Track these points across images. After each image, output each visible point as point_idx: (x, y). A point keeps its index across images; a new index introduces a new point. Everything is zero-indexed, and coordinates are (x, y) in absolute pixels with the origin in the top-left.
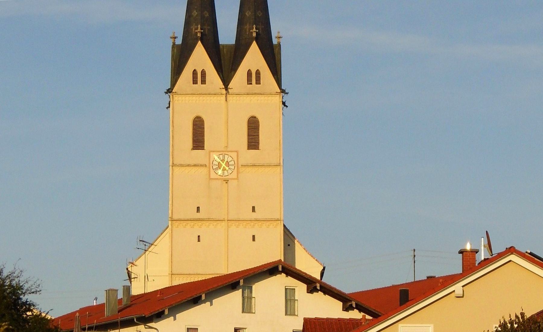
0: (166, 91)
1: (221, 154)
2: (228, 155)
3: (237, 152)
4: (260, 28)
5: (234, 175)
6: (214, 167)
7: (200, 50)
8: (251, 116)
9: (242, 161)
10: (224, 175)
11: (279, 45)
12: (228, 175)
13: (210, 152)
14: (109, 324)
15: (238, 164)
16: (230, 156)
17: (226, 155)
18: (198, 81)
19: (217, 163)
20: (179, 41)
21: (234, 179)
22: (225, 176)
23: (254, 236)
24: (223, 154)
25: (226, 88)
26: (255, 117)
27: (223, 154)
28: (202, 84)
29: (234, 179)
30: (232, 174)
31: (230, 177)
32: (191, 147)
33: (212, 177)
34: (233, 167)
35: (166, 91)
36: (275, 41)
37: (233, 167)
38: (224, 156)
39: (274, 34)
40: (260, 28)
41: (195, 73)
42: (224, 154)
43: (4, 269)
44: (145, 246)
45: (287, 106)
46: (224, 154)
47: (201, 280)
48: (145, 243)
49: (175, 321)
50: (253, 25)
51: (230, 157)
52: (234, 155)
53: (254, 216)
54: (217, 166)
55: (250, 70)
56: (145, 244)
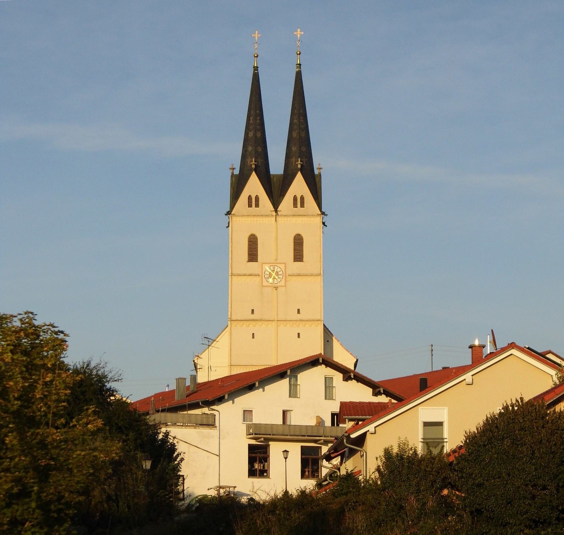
0: (226, 213)
3: (285, 263)
5: (282, 283)
9: (289, 272)
11: (320, 175)
13: (263, 264)
15: (285, 274)
17: (276, 266)
19: (269, 273)
20: (237, 172)
23: (299, 334)
26: (300, 235)
34: (281, 277)
35: (226, 213)
36: (316, 172)
37: (281, 277)
38: (274, 267)
39: (316, 166)
41: (250, 198)
45: (326, 226)
52: (282, 266)
53: (299, 317)
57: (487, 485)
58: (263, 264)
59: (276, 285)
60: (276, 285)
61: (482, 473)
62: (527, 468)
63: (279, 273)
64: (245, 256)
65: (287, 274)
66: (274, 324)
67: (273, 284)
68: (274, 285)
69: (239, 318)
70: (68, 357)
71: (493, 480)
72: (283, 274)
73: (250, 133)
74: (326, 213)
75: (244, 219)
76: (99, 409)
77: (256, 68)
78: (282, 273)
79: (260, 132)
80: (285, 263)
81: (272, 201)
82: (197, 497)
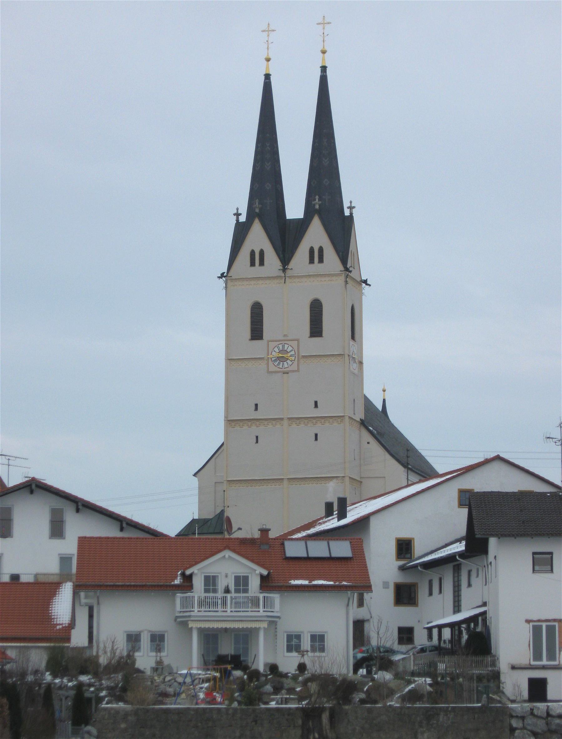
0: (220, 276)
1: (281, 344)
2: (288, 345)
3: (298, 340)
4: (327, 199)
5: (295, 367)
7: (257, 229)
8: (312, 300)
11: (351, 216)
14: (513, 536)
15: (298, 355)
17: (285, 345)
19: (288, 350)
20: (243, 219)
21: (293, 371)
22: (284, 368)
23: (316, 435)
24: (282, 344)
25: (284, 270)
29: (293, 371)
30: (292, 366)
31: (290, 369)
35: (220, 276)
36: (347, 213)
38: (284, 345)
39: (346, 204)
40: (327, 199)
44: (8, 460)
45: (370, 285)
48: (7, 458)
49: (268, 527)
50: (316, 196)
51: (274, 349)
56: (8, 458)
58: (268, 341)
59: (285, 370)
60: (285, 370)
64: (247, 333)
65: (300, 356)
69: (10, 469)
70: (386, 388)
72: (295, 354)
73: (266, 163)
77: (324, 69)
78: (294, 354)
79: (270, 163)
81: (282, 256)
82: (443, 579)
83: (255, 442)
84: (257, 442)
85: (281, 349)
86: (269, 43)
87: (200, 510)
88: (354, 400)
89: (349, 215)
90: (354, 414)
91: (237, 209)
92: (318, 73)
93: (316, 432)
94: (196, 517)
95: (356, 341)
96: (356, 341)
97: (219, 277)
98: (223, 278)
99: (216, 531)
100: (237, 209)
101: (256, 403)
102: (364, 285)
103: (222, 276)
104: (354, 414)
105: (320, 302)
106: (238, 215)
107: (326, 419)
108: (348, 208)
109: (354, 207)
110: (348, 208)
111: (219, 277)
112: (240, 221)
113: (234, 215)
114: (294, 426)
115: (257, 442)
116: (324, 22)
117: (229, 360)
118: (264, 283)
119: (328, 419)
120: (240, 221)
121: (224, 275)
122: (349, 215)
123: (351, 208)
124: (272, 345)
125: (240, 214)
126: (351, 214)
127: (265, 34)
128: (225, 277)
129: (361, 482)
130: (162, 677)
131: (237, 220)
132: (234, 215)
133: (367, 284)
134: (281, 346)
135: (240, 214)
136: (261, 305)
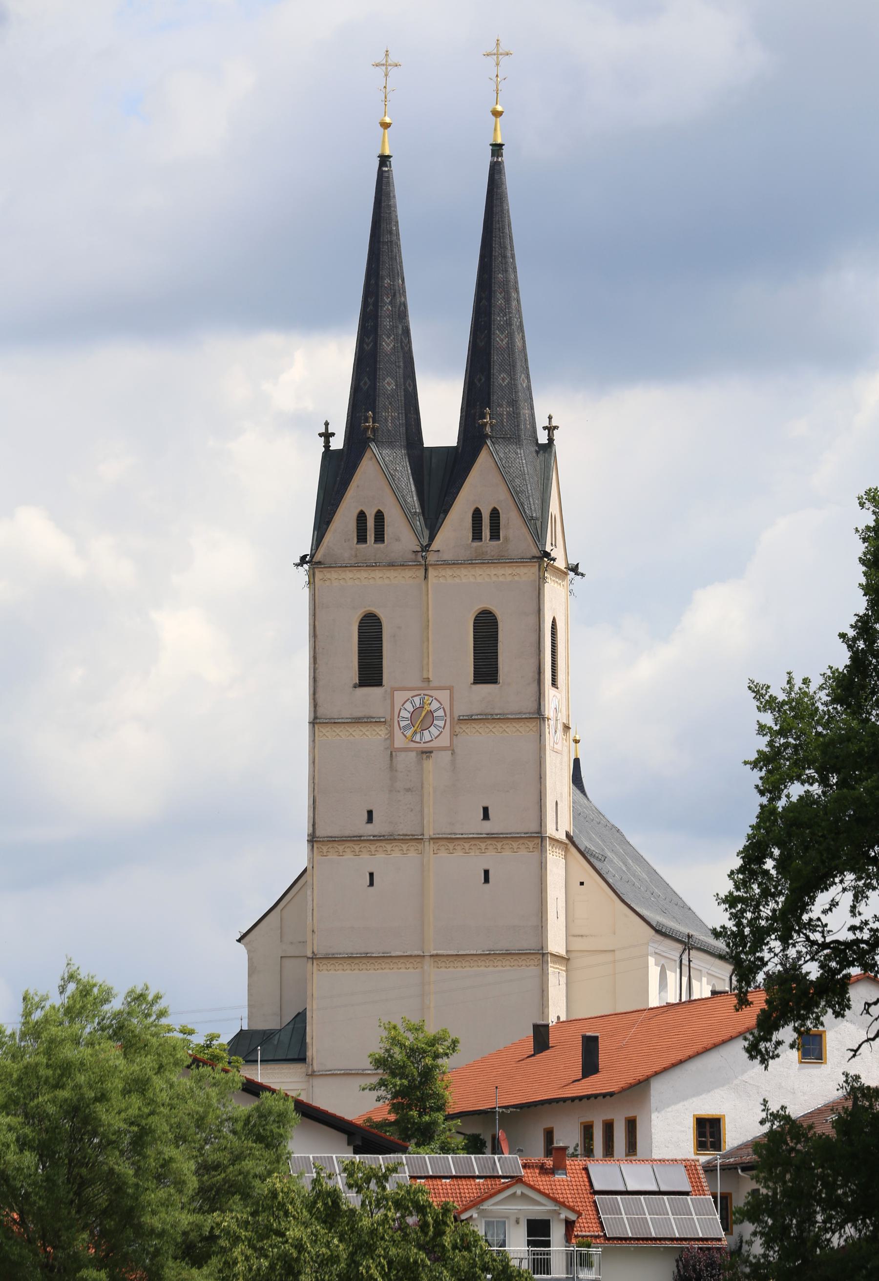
0: (757, 1061)
3: (451, 689)
6: (402, 724)
8: (479, 612)
9: (462, 709)
10: (423, 740)
12: (432, 740)
13: (394, 689)
16: (435, 699)
18: (368, 537)
20: (337, 443)
22: (424, 743)
24: (420, 695)
26: (490, 613)
27: (420, 695)
28: (376, 541)
32: (472, 681)
33: (397, 744)
34: (441, 723)
35: (757, 1061)
36: (543, 438)
37: (441, 723)
39: (541, 422)
41: (361, 517)
42: (422, 696)
43: (803, 967)
45: (582, 575)
46: (422, 696)
47: (817, 978)
52: (444, 696)
53: (487, 827)
54: (435, 722)
55: (364, 513)
57: (777, 950)
58: (394, 689)
61: (820, 929)
62: (268, 1232)
63: (435, 714)
66: (429, 832)
67: (398, 717)
68: (422, 745)
71: (250, 1233)
74: (580, 570)
75: (348, 575)
76: (815, 1212)
80: (451, 689)
83: (368, 884)
84: (371, 884)
85: (418, 706)
86: (388, 90)
87: (250, 1017)
88: (557, 802)
89: (547, 442)
90: (557, 830)
91: (327, 424)
92: (487, 158)
93: (486, 868)
94: (245, 1028)
95: (557, 688)
96: (557, 688)
97: (297, 565)
98: (305, 565)
99: (289, 1057)
100: (327, 424)
101: (369, 808)
102: (572, 574)
103: (303, 560)
104: (557, 830)
105: (494, 616)
106: (327, 436)
107: (505, 842)
108: (545, 428)
109: (556, 428)
110: (545, 428)
111: (297, 565)
112: (331, 448)
113: (321, 435)
114: (443, 854)
115: (371, 884)
116: (497, 51)
117: (315, 722)
118: (385, 577)
119: (526, 841)
120: (331, 448)
121: (307, 559)
122: (547, 442)
123: (550, 429)
124: (399, 697)
125: (333, 434)
126: (551, 440)
127: (381, 71)
128: (307, 563)
129: (568, 959)
130: (773, 828)
131: (327, 446)
132: (321, 435)
133: (577, 574)
134: (440, 713)
135: (333, 434)
136: (379, 619)
